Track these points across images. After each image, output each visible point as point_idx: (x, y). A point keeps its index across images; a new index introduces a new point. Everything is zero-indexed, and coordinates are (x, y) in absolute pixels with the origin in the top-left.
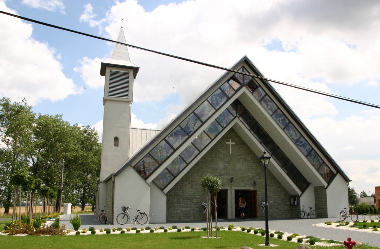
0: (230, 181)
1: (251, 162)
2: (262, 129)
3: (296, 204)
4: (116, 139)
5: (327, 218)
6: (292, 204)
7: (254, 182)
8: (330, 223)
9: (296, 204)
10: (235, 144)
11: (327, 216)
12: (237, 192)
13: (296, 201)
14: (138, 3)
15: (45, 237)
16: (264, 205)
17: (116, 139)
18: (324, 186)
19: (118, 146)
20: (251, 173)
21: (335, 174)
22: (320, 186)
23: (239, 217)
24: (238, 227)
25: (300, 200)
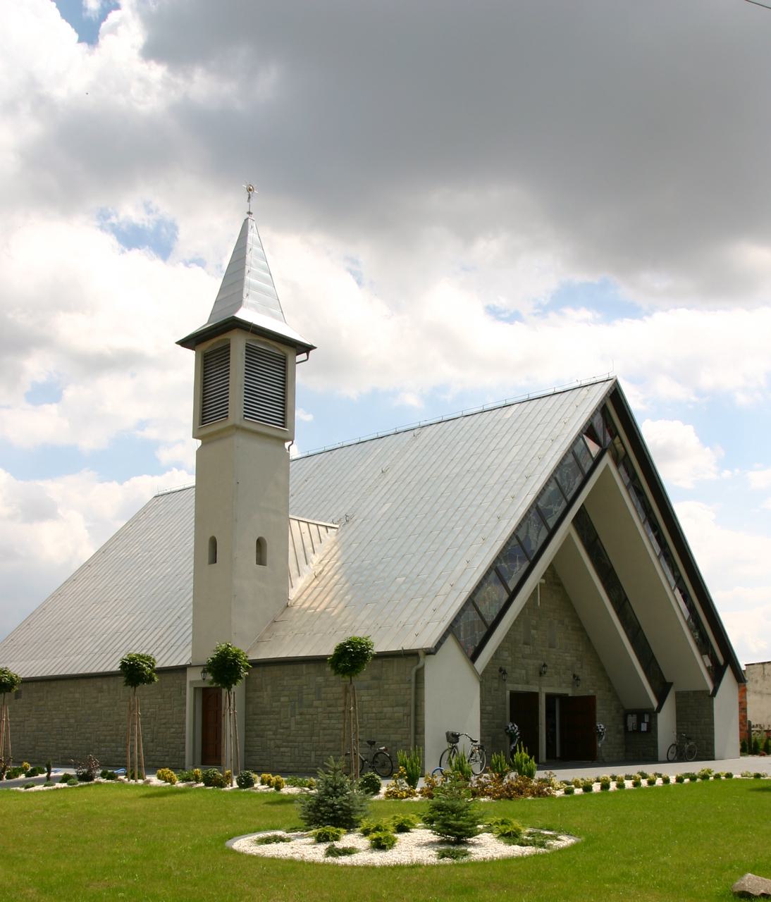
0: (538, 673)
1: (570, 628)
2: (604, 553)
3: (644, 727)
4: (260, 543)
5: (714, 760)
6: (630, 729)
7: (574, 676)
8: (125, 764)
9: (644, 727)
10: (546, 582)
11: (714, 755)
12: (154, 680)
13: (644, 722)
14: (80, 41)
15: (47, 791)
16: (602, 729)
17: (260, 543)
18: (709, 691)
19: (265, 565)
20: (569, 655)
21: (723, 667)
22: (694, 690)
23: (681, 755)
24: (672, 771)
25: (656, 724)
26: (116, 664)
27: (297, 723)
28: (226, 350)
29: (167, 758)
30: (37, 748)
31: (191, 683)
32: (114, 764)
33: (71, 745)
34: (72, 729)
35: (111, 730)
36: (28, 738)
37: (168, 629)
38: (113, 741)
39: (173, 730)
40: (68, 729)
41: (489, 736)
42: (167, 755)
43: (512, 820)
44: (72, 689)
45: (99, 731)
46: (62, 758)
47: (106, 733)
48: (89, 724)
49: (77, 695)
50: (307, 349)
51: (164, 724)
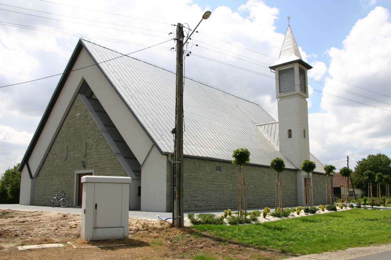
4: (290, 136)
17: (290, 136)
26: (267, 163)
27: (316, 191)
28: (293, 69)
29: (289, 202)
30: (232, 200)
31: (304, 176)
32: (271, 206)
33: (252, 198)
34: (252, 190)
35: (270, 191)
36: (226, 195)
37: (207, 152)
38: (271, 196)
39: (290, 192)
40: (250, 190)
41: (2, 213)
42: (289, 201)
43: (329, 212)
44: (252, 171)
45: (265, 191)
46: (248, 205)
47: (268, 192)
48: (261, 188)
49: (255, 174)
50: (80, 47)
51: (288, 189)
